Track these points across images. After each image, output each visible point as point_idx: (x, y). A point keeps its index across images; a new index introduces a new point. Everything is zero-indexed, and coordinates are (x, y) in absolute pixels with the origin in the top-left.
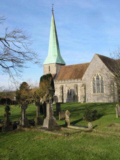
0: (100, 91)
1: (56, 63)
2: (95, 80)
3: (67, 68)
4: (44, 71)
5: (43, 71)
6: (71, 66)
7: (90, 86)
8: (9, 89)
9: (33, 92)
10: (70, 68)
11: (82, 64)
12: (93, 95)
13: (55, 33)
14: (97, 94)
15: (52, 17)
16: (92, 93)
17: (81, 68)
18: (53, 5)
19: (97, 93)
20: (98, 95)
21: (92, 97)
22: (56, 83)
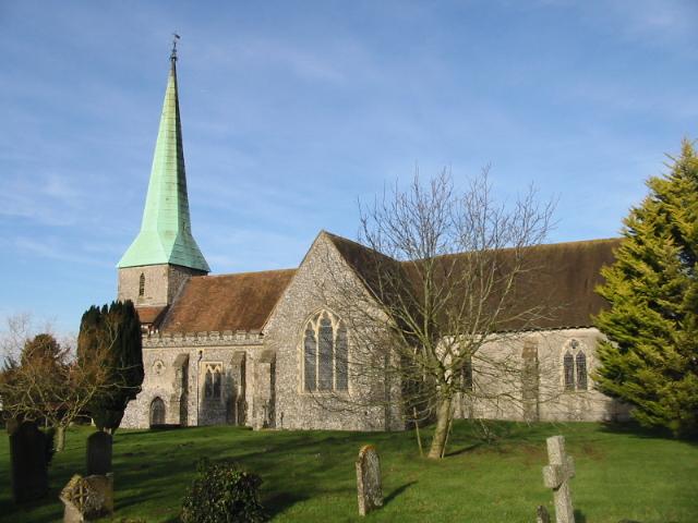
1: (170, 264)
7: (295, 362)
10: (225, 285)
15: (170, 84)
18: (178, 37)
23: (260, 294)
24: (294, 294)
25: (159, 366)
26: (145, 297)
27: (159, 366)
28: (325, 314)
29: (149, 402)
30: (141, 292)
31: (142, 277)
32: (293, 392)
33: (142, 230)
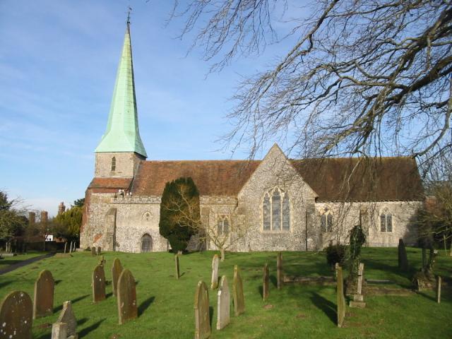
0: (280, 227)
1: (135, 152)
2: (271, 200)
3: (160, 168)
4: (96, 169)
5: (94, 168)
6: (172, 162)
7: (258, 215)
8: (404, 224)
9: (408, 231)
10: (169, 167)
11: (199, 162)
12: (264, 235)
13: (131, 79)
14: (274, 232)
15: (127, 40)
16: (261, 229)
17: (199, 171)
18: (131, 9)
19: (273, 229)
20: (275, 234)
21: (261, 239)
22: (149, 202)
23: (196, 174)
24: (256, 177)
25: (148, 215)
26: (116, 172)
27: (148, 215)
28: (277, 189)
29: (140, 236)
30: (113, 168)
31: (114, 159)
32: (257, 231)
33: (112, 129)
